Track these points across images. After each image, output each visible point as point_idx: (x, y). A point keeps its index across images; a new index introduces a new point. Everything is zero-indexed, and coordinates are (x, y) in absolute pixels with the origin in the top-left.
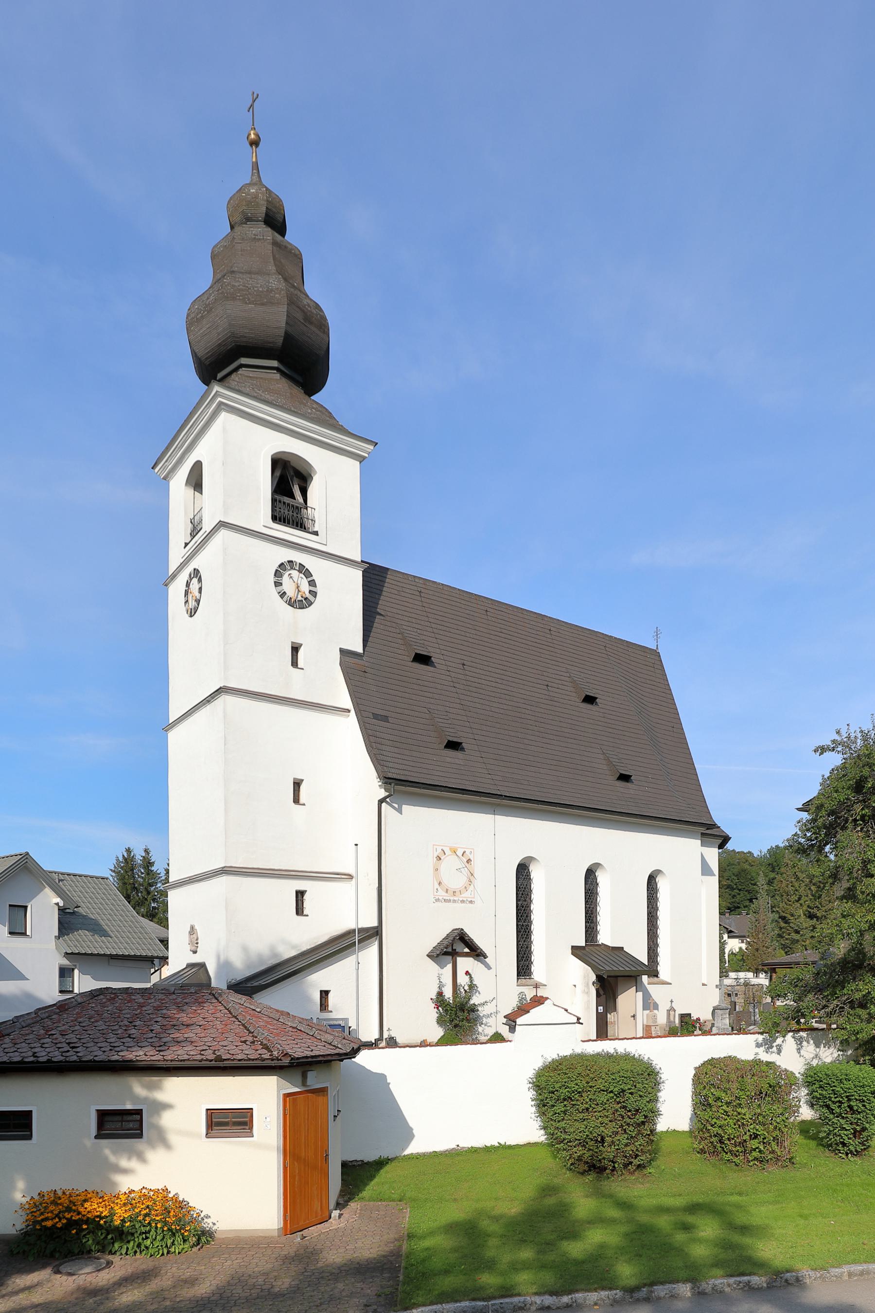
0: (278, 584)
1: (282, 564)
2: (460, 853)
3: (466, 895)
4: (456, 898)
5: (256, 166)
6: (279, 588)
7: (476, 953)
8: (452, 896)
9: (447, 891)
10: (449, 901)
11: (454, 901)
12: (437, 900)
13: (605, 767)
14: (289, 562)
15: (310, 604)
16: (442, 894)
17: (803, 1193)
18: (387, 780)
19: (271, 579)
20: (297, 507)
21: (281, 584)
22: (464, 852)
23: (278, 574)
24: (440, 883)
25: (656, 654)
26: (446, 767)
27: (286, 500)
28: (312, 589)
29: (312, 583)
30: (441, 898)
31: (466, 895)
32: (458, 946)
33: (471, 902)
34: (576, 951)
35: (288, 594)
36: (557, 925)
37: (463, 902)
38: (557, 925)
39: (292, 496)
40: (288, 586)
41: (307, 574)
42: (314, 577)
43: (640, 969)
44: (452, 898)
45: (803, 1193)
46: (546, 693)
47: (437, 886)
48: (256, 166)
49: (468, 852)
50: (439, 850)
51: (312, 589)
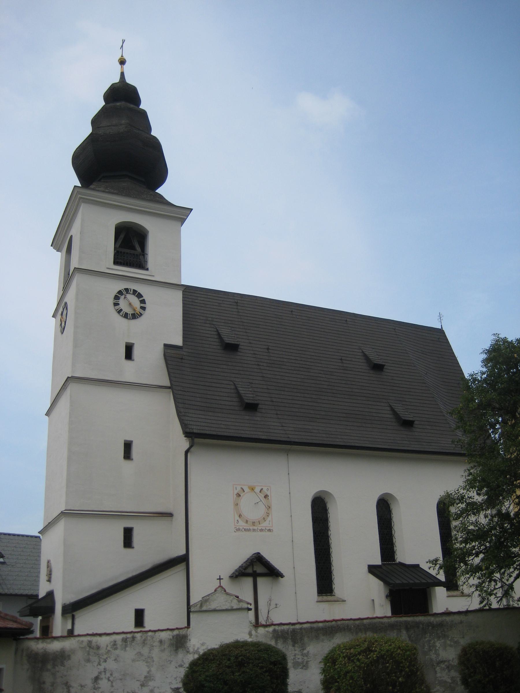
0: (116, 304)
1: (120, 291)
2: (257, 490)
3: (264, 525)
4: (255, 528)
5: (122, 74)
6: (117, 307)
7: (273, 573)
8: (253, 526)
9: (247, 522)
10: (249, 530)
11: (254, 530)
12: (238, 530)
13: (391, 416)
14: (125, 289)
15: (141, 315)
16: (242, 524)
17: (252, 648)
18: (188, 434)
19: (111, 301)
20: (137, 255)
21: (118, 304)
22: (262, 490)
23: (116, 298)
24: (240, 516)
25: (440, 332)
26: (243, 423)
27: (132, 252)
28: (143, 305)
29: (143, 302)
30: (241, 528)
31: (264, 525)
32: (258, 569)
33: (269, 530)
34: (372, 569)
35: (124, 310)
36: (355, 546)
37: (262, 530)
38: (355, 546)
39: (133, 248)
40: (123, 304)
41: (139, 296)
42: (144, 298)
43: (430, 581)
44: (251, 528)
45: (252, 648)
46: (340, 364)
47: (237, 517)
48: (122, 74)
49: (265, 489)
50: (239, 488)
51: (143, 305)
